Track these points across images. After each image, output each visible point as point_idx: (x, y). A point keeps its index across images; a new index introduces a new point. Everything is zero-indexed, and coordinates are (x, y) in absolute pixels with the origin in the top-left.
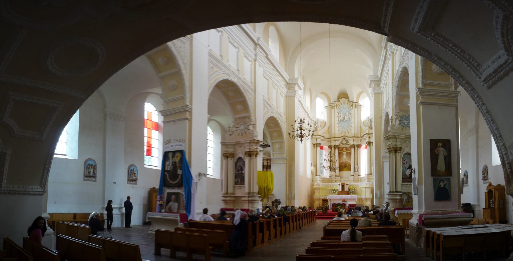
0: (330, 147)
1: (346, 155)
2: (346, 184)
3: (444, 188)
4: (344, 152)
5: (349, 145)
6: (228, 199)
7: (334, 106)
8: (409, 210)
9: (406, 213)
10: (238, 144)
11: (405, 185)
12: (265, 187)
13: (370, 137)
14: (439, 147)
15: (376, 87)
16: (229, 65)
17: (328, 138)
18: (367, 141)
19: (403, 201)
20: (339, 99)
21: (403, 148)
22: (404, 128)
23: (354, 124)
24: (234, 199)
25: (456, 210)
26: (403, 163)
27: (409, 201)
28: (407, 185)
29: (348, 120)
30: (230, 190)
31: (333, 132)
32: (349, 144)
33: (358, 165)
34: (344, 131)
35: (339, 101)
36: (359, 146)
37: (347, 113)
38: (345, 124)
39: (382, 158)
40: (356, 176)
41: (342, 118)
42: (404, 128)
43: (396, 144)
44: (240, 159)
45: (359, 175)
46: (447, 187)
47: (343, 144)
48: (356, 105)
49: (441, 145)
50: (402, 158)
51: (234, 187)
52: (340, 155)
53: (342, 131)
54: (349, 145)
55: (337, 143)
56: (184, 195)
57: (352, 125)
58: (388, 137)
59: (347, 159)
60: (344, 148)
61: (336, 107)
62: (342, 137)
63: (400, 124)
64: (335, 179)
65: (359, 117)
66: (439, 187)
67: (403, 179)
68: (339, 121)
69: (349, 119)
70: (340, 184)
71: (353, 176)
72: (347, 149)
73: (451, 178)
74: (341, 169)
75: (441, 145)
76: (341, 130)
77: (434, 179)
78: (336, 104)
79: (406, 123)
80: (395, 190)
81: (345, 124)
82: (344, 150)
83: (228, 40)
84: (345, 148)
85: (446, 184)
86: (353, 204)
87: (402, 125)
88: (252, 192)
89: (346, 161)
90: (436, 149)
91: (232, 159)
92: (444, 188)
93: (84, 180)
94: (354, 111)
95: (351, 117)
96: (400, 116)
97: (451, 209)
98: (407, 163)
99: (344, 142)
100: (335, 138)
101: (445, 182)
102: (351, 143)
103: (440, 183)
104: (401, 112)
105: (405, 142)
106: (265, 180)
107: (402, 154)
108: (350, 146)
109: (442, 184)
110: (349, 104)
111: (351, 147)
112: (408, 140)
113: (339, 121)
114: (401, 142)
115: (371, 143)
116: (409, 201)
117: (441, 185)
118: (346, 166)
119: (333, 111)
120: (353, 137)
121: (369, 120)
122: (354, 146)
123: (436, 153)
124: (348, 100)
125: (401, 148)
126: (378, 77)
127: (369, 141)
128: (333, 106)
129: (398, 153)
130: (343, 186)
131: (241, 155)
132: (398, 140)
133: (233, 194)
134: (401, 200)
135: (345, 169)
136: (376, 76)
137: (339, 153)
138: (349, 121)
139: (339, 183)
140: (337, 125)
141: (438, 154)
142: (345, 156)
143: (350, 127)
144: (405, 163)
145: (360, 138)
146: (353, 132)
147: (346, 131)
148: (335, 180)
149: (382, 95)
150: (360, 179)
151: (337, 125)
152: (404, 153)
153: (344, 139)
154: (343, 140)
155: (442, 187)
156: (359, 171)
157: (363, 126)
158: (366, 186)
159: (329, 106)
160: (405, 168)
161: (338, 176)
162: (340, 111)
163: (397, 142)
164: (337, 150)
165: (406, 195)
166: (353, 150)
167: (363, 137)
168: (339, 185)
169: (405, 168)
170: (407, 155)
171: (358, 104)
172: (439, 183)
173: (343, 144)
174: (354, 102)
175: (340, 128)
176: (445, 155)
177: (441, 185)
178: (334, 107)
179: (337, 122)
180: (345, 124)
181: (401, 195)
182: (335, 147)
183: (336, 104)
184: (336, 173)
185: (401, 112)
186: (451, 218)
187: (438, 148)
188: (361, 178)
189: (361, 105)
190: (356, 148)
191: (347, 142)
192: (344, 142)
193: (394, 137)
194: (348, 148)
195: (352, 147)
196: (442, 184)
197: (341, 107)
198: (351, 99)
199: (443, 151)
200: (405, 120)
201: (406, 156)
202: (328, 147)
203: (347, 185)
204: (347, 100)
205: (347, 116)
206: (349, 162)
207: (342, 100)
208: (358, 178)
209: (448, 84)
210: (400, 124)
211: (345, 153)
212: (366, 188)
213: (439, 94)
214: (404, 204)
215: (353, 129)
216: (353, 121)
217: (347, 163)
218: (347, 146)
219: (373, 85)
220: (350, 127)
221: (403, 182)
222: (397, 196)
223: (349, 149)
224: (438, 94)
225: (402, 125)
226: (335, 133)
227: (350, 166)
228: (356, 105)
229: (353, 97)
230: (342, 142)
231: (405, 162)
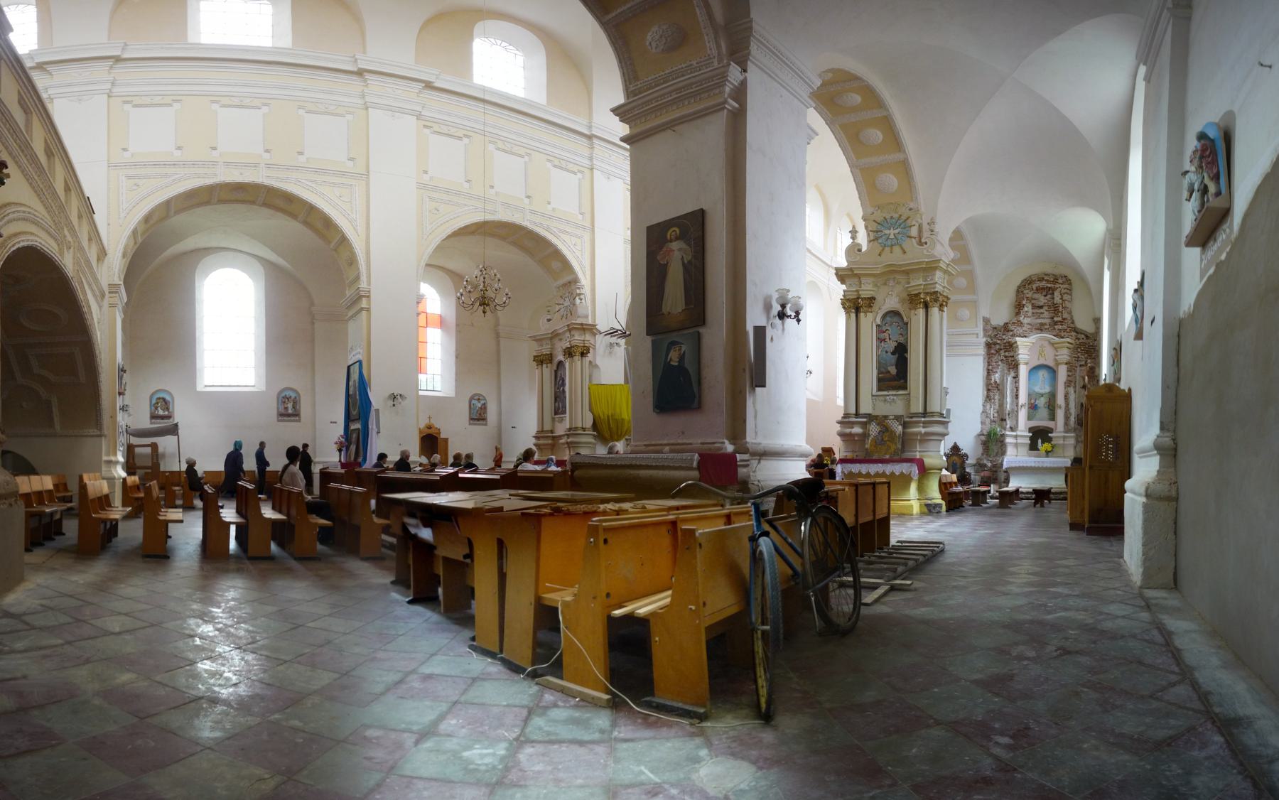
3: (681, 369)
6: (542, 442)
8: (871, 465)
9: (864, 473)
10: (555, 336)
11: (882, 398)
12: (608, 417)
14: (671, 241)
16: (554, 210)
19: (868, 439)
21: (879, 298)
24: (550, 442)
25: (714, 443)
26: (880, 340)
27: (882, 440)
28: (888, 398)
30: (547, 427)
42: (887, 249)
43: (857, 291)
44: (560, 364)
46: (688, 365)
49: (676, 234)
50: (878, 326)
51: (553, 419)
63: (873, 240)
66: (668, 367)
67: (879, 380)
73: (702, 330)
75: (676, 234)
77: (653, 342)
79: (892, 236)
80: (854, 412)
83: (549, 165)
85: (686, 354)
87: (880, 243)
88: (573, 426)
90: (661, 248)
91: (549, 365)
92: (681, 369)
93: (470, 424)
96: (874, 221)
97: (699, 442)
98: (890, 339)
101: (684, 348)
103: (668, 355)
104: (879, 211)
105: (885, 284)
106: (610, 403)
109: (674, 356)
112: (895, 278)
114: (876, 286)
116: (882, 440)
117: (671, 360)
123: (662, 262)
125: (872, 299)
131: (561, 357)
132: (863, 280)
133: (552, 433)
134: (865, 436)
141: (668, 263)
144: (884, 340)
155: (676, 364)
160: (887, 352)
163: (862, 285)
165: (878, 424)
169: (887, 352)
170: (891, 317)
172: (667, 354)
176: (686, 262)
177: (671, 360)
181: (864, 425)
185: (879, 211)
186: (641, 465)
187: (667, 245)
193: (850, 273)
196: (674, 356)
199: (680, 250)
200: (890, 229)
201: (888, 319)
209: (697, 63)
210: (873, 240)
213: (670, 98)
214: (867, 449)
221: (879, 389)
222: (854, 426)
224: (667, 100)
231: (886, 335)
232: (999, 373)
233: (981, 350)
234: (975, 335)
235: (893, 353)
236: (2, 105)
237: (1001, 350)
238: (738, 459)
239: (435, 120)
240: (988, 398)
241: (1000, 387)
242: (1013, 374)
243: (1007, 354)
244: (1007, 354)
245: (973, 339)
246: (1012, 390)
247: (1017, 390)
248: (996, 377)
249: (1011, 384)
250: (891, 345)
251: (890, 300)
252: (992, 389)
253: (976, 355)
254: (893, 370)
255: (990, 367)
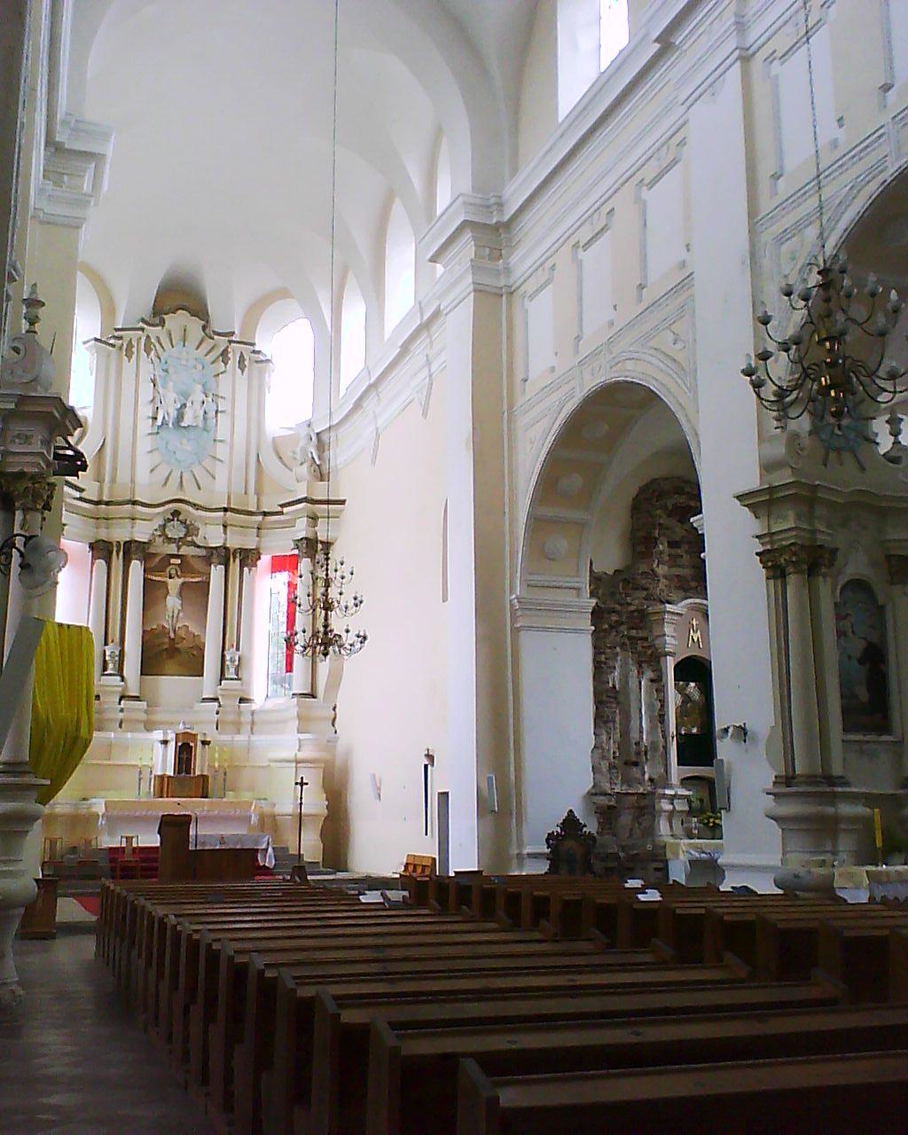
0: (101, 549)
1: (180, 594)
2: (200, 738)
4: (170, 581)
5: (199, 547)
7: (135, 343)
13: (314, 519)
15: (483, 258)
17: (97, 503)
18: (302, 535)
20: (159, 312)
22: (833, 456)
23: (232, 447)
29: (201, 425)
31: (123, 476)
32: (198, 540)
33: (238, 649)
34: (176, 475)
35: (162, 323)
36: (248, 557)
37: (199, 387)
38: (181, 444)
39: (513, 611)
40: (230, 704)
41: (173, 414)
45: (242, 700)
47: (170, 540)
48: (242, 356)
52: (152, 591)
53: (167, 474)
54: (199, 547)
55: (142, 532)
56: (236, 797)
57: (222, 451)
58: (770, 494)
59: (181, 614)
60: (173, 561)
61: (148, 351)
62: (167, 507)
64: (122, 710)
65: (254, 414)
68: (159, 422)
69: (205, 419)
70: (171, 736)
71: (216, 699)
72: (185, 566)
74: (150, 666)
76: (162, 473)
78: (148, 337)
81: (181, 444)
82: (173, 572)
84: (179, 561)
86: (140, 845)
89: (179, 625)
94: (232, 383)
95: (217, 412)
99: (175, 531)
100: (135, 503)
102: (213, 536)
107: (836, 585)
108: (203, 552)
110: (208, 343)
111: (208, 560)
113: (159, 422)
115: (320, 546)
118: (178, 650)
119: (129, 367)
120: (225, 510)
121: (314, 438)
122: (224, 555)
124: (204, 328)
126: (500, 205)
127: (310, 536)
128: (130, 344)
129: (824, 577)
130: (185, 752)
135: (170, 665)
136: (492, 201)
137: (148, 585)
138: (204, 429)
139: (165, 734)
140: (144, 444)
142: (173, 602)
143: (207, 463)
145: (260, 518)
146: (219, 489)
147: (186, 476)
148: (121, 715)
149: (510, 305)
150: (246, 718)
151: (144, 444)
152: (843, 580)
153: (176, 513)
154: (170, 521)
156: (243, 674)
157: (269, 461)
158: (301, 755)
159: (112, 341)
160: (850, 657)
161: (137, 698)
162: (163, 374)
164: (136, 567)
166: (216, 572)
167: (281, 513)
168: (165, 742)
169: (850, 657)
171: (254, 352)
173: (170, 540)
174: (234, 338)
175: (157, 458)
178: (134, 350)
179: (145, 426)
180: (185, 441)
182: (131, 549)
183: (148, 337)
184: (123, 679)
188: (253, 713)
189: (268, 361)
190: (235, 566)
191: (190, 529)
192: (175, 531)
194: (192, 561)
195: (215, 560)
197: (170, 356)
198: (216, 326)
202: (92, 546)
203: (204, 743)
204: (203, 323)
205: (197, 405)
206: (193, 629)
207: (176, 321)
208: (240, 713)
211: (174, 584)
212: (297, 762)
215: (221, 473)
216: (222, 431)
217: (182, 633)
218: (184, 550)
219: (466, 248)
220: (207, 463)
223: (198, 565)
225: (823, 436)
226: (133, 481)
227: (202, 650)
228: (242, 356)
229: (226, 310)
230: (164, 526)
232: (618, 670)
233: (586, 624)
234: (574, 592)
235: (861, 661)
236: (656, 5)
237: (622, 623)
238: (194, 849)
239: (698, 92)
240: (601, 720)
241: (621, 698)
242: (649, 674)
243: (633, 633)
244: (633, 633)
245: (568, 597)
246: (650, 706)
247: (662, 706)
248: (615, 678)
249: (649, 693)
250: (857, 646)
251: (856, 565)
252: (608, 703)
253: (576, 631)
254: (863, 694)
255: (603, 658)
